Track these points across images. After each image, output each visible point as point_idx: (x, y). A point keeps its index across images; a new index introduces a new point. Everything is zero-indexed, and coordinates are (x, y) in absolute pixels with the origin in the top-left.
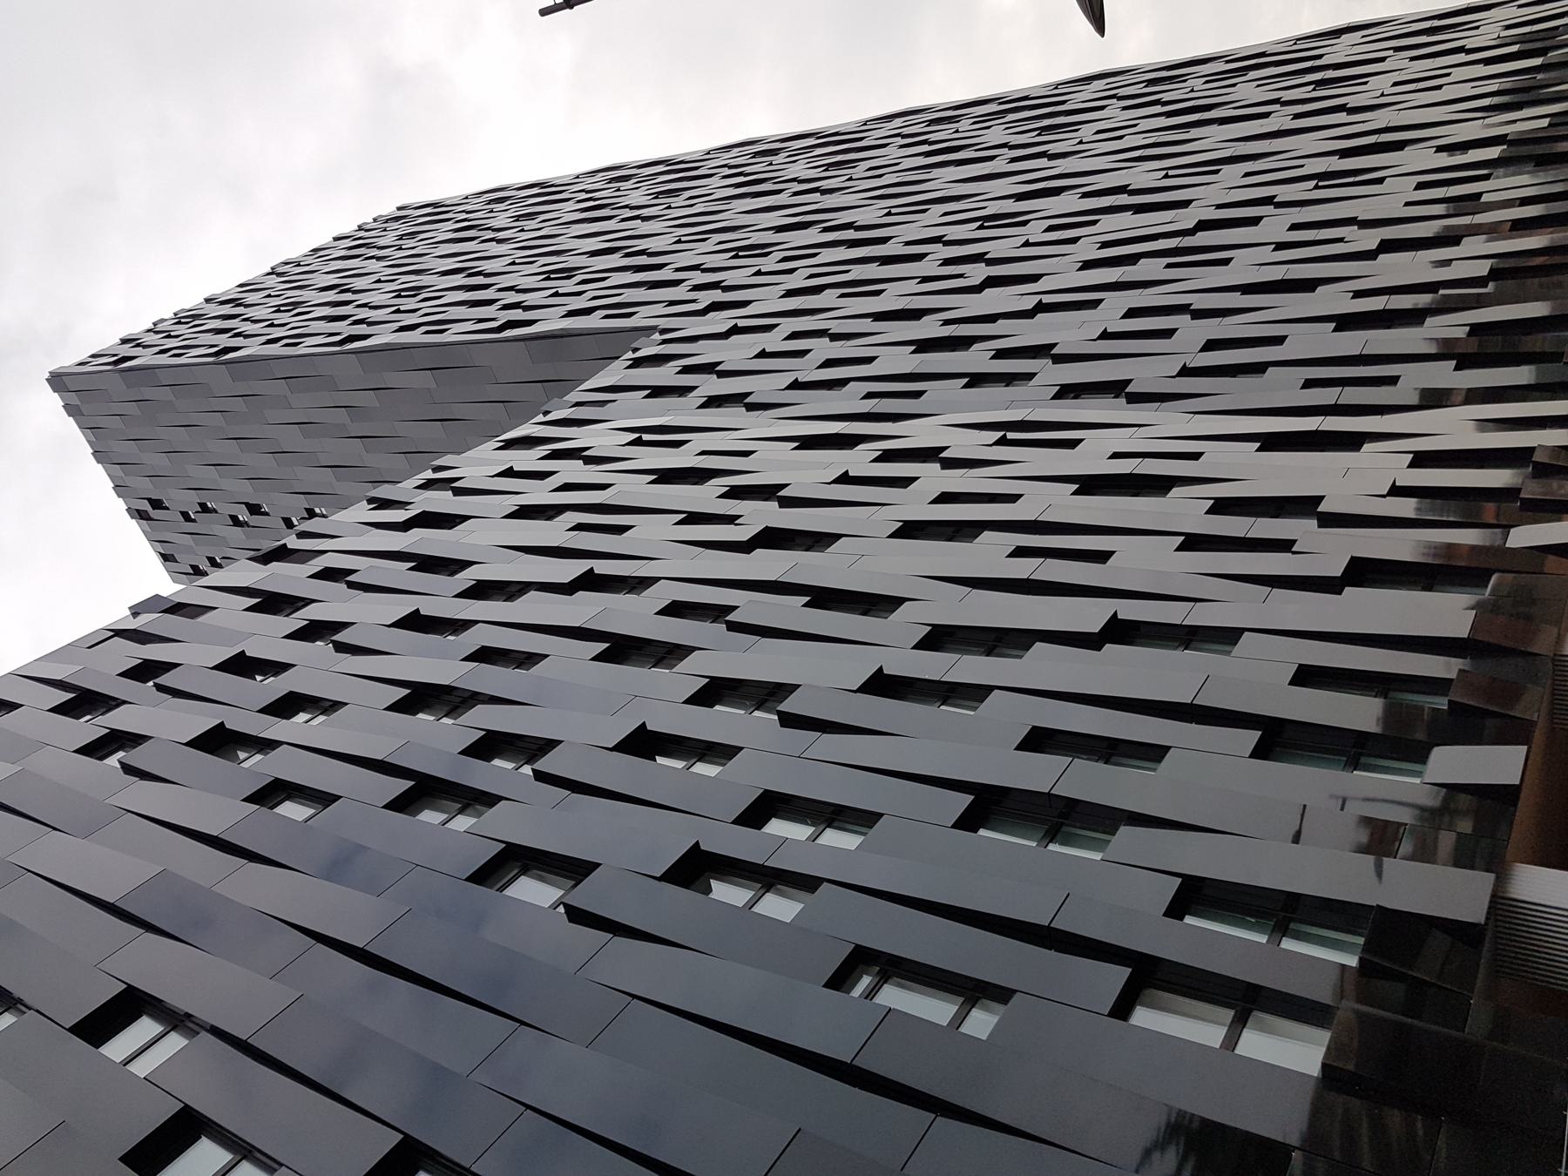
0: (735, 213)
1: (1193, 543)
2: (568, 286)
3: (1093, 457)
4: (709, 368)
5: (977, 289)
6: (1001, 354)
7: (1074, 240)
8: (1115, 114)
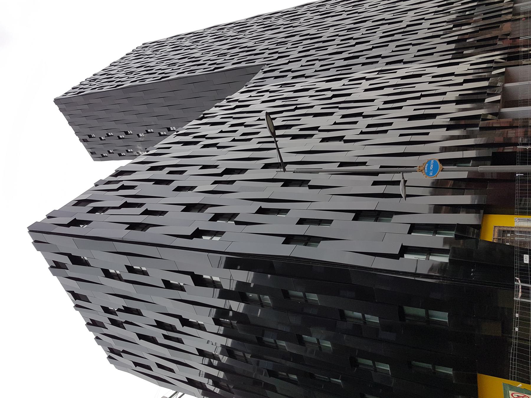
0: (216, 46)
1: (430, 83)
2: (132, 76)
3: (298, 87)
4: (289, 71)
5: (354, 46)
6: (367, 58)
7: (375, 32)
8: (309, 15)
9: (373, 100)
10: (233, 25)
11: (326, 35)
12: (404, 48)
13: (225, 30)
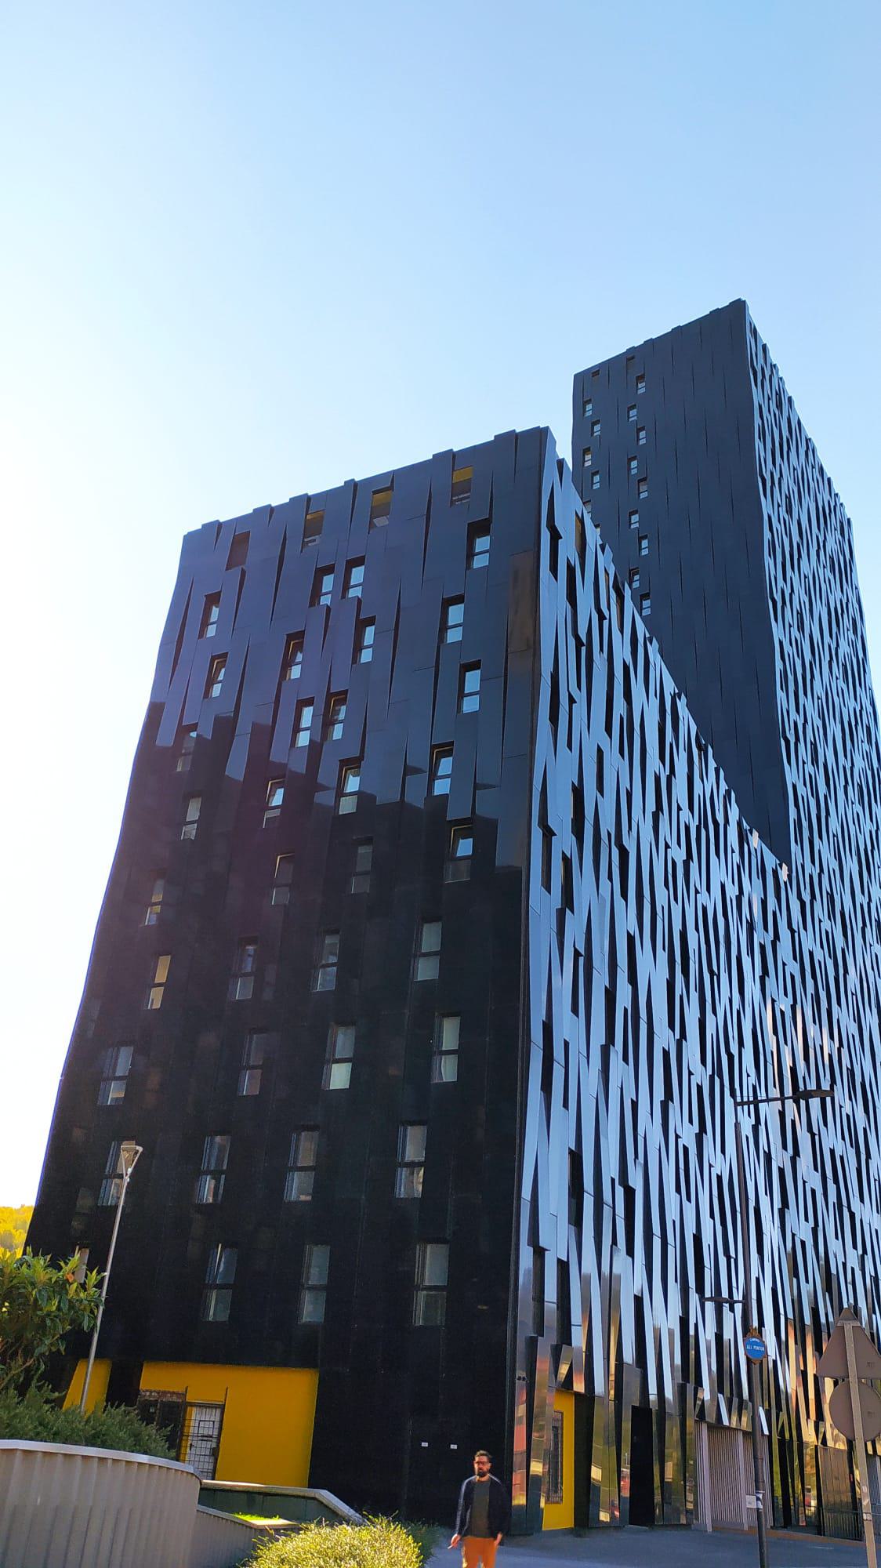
0: (820, 609)
2: (773, 406)
7: (843, 1138)
8: (868, 826)
9: (723, 1151)
10: (861, 656)
11: (823, 848)
12: (791, 988)
13: (852, 636)
